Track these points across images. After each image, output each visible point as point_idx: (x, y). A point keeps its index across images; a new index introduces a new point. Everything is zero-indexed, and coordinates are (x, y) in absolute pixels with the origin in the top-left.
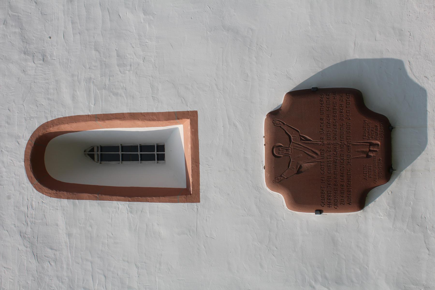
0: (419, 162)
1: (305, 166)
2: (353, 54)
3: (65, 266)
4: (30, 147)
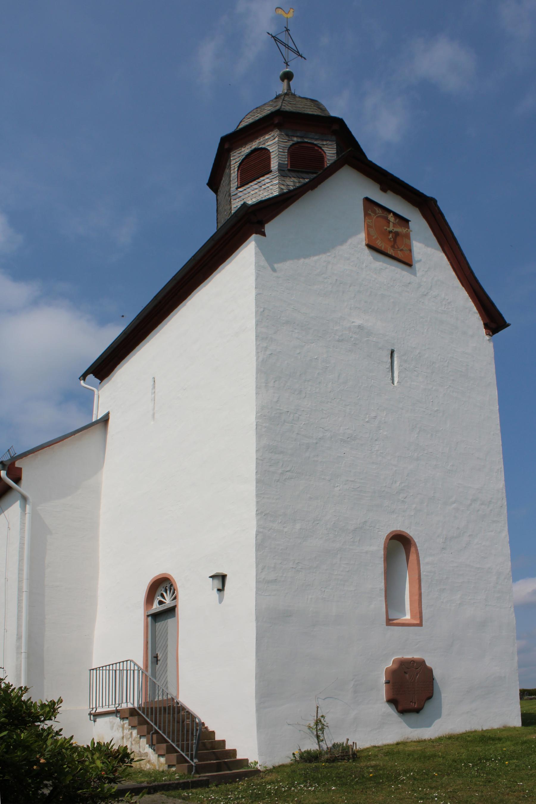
0: (404, 724)
1: (407, 676)
2: (443, 695)
3: (351, 547)
4: (406, 535)
